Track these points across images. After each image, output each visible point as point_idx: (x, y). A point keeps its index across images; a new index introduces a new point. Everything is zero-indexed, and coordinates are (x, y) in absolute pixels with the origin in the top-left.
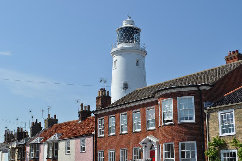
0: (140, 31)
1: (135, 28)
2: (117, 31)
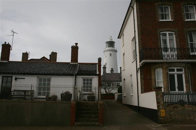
1: (112, 42)
2: (106, 42)
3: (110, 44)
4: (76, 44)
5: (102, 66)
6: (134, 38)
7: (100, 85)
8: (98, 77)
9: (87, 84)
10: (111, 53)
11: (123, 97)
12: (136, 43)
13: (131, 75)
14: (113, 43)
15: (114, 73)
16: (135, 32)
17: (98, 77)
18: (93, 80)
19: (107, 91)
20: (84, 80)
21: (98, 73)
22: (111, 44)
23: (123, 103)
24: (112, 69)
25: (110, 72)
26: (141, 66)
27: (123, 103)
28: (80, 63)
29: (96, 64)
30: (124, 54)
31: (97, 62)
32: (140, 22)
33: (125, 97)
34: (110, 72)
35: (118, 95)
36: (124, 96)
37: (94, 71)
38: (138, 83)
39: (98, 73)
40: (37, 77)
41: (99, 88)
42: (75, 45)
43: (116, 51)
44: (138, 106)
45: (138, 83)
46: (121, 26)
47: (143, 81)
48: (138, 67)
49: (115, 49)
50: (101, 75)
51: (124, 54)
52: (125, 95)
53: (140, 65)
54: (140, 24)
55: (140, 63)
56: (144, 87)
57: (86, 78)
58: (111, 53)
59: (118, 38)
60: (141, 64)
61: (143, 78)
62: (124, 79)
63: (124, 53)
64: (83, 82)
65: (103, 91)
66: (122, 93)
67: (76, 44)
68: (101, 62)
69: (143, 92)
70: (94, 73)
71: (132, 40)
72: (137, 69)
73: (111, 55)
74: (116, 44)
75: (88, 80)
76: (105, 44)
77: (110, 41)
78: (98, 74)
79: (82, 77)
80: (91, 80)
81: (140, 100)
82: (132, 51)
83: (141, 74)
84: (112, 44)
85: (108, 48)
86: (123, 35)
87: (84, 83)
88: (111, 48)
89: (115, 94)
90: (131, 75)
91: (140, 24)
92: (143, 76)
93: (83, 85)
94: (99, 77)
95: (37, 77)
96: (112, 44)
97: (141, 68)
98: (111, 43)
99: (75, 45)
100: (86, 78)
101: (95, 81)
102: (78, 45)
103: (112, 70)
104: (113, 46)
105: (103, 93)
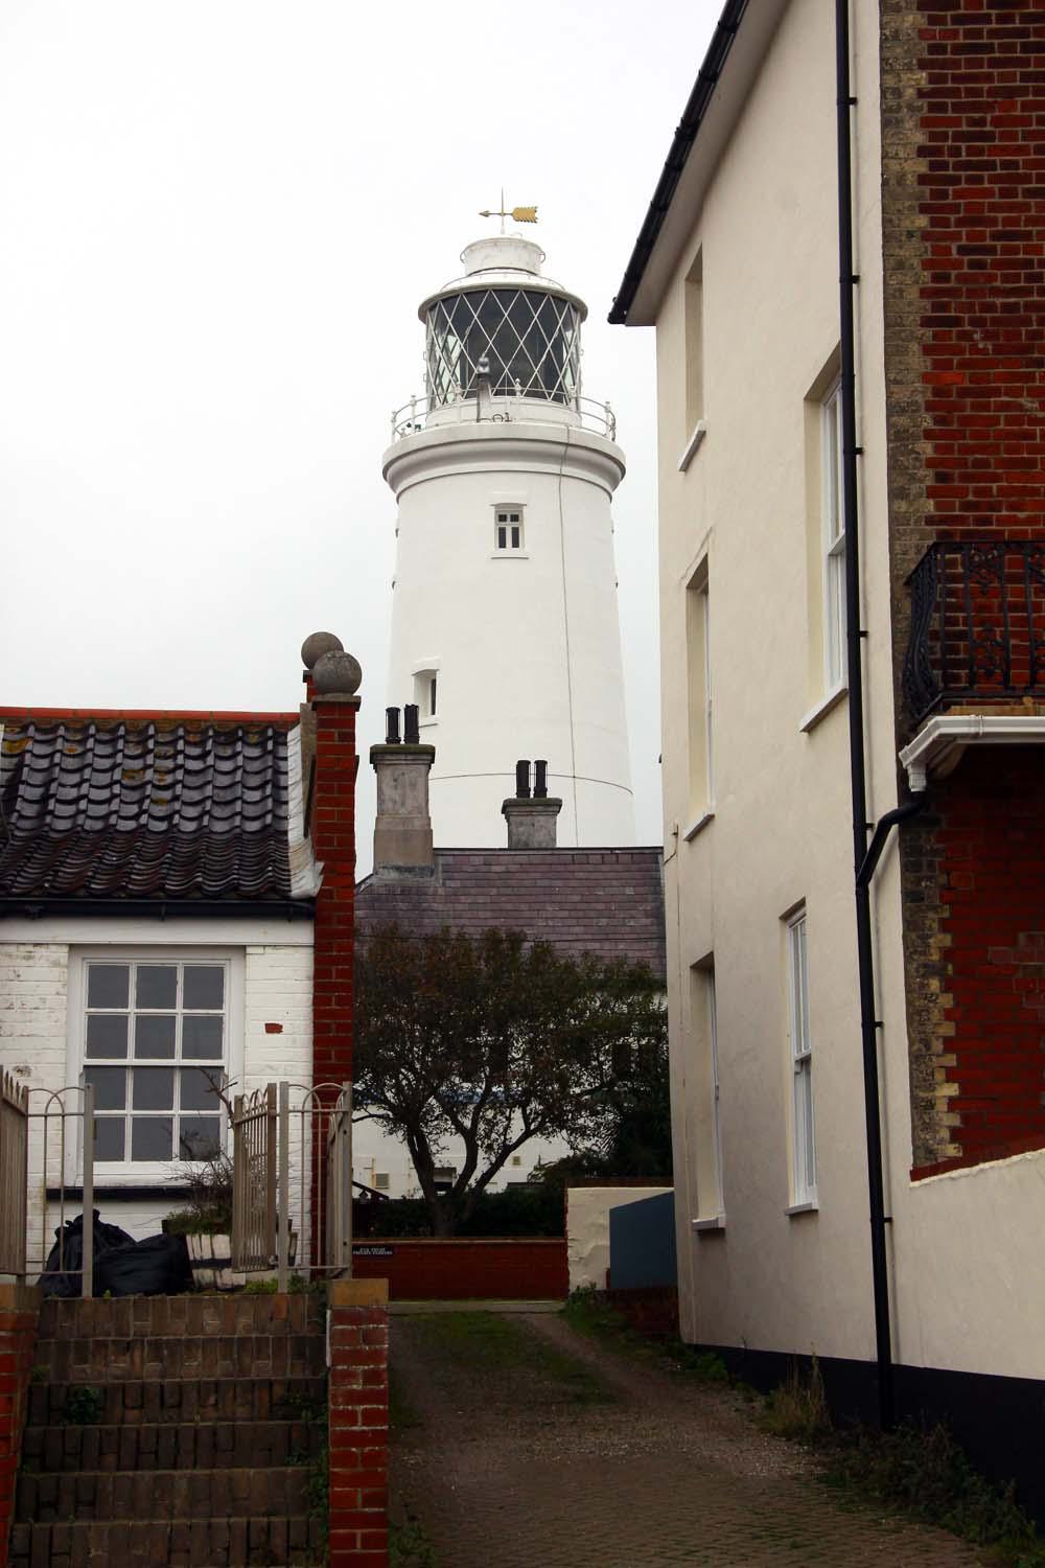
0: (583, 317)
1: (537, 294)
2: (428, 309)
3: (506, 344)
5: (369, 731)
6: (838, 378)
7: (345, 1051)
8: (303, 934)
9: (155, 1036)
11: (686, 1245)
12: (852, 452)
13: (793, 915)
14: (549, 321)
15: (564, 840)
16: (849, 280)
17: (303, 934)
19: (450, 1151)
20: (105, 985)
21: (305, 880)
22: (502, 333)
23: (691, 1329)
26: (917, 783)
27: (691, 1329)
29: (267, 730)
31: (287, 694)
32: (920, 138)
33: (711, 1234)
34: (493, 834)
37: (237, 838)
38: (870, 1025)
39: (305, 880)
40: (83, 959)
41: (324, 1097)
44: (867, 1352)
45: (870, 1025)
46: (669, 139)
47: (947, 1001)
48: (884, 800)
49: (590, 426)
50: (359, 876)
52: (711, 1210)
53: (902, 777)
54: (922, 166)
55: (902, 740)
56: (952, 1090)
60: (928, 761)
61: (947, 954)
62: (705, 968)
63: (705, 560)
64: (93, 1021)
65: (378, 1155)
66: (665, 1175)
68: (352, 724)
69: (952, 1150)
70: (250, 885)
71: (816, 397)
72: (860, 825)
75: (157, 985)
78: (310, 899)
79: (73, 947)
80: (208, 987)
81: (903, 1275)
83: (911, 896)
84: (537, 344)
85: (462, 417)
86: (696, 278)
87: (104, 1035)
90: (793, 915)
91: (922, 166)
92: (945, 926)
93: (80, 1059)
94: (321, 950)
95: (80, 960)
96: (537, 344)
97: (912, 812)
98: (521, 317)
100: (180, 963)
101: (268, 996)
103: (531, 797)
104: (551, 375)
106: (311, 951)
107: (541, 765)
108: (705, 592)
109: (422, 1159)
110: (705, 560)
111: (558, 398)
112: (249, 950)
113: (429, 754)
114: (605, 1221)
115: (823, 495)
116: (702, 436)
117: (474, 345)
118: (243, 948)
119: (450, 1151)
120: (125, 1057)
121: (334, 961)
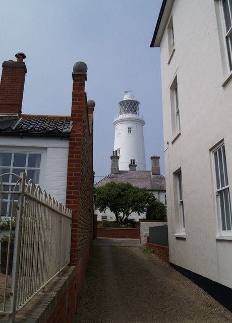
1: (133, 101)
3: (129, 107)
4: (21, 56)
8: (65, 144)
10: (130, 125)
14: (135, 104)
18: (42, 156)
24: (133, 162)
25: (128, 169)
28: (25, 117)
30: (174, 87)
35: (151, 229)
36: (177, 234)
42: (15, 60)
43: (142, 123)
51: (174, 87)
57: (13, 152)
58: (130, 125)
59: (152, 46)
62: (178, 174)
67: (21, 56)
73: (129, 130)
74: (141, 107)
75: (20, 160)
76: (118, 107)
77: (129, 101)
80: (35, 160)
82: (220, 39)
86: (171, 27)
88: (130, 116)
89: (142, 223)
94: (71, 149)
99: (15, 60)
102: (24, 60)
103: (132, 165)
105: (111, 218)
106: (68, 149)
107: (134, 160)
108: (176, 90)
109: (117, 216)
110: (176, 77)
111: (136, 114)
112: (48, 149)
113: (118, 157)
114: (148, 229)
115: (223, 27)
116: (174, 50)
117: (125, 107)
118: (46, 148)
119: (121, 214)
120: (8, 182)
121: (75, 152)
